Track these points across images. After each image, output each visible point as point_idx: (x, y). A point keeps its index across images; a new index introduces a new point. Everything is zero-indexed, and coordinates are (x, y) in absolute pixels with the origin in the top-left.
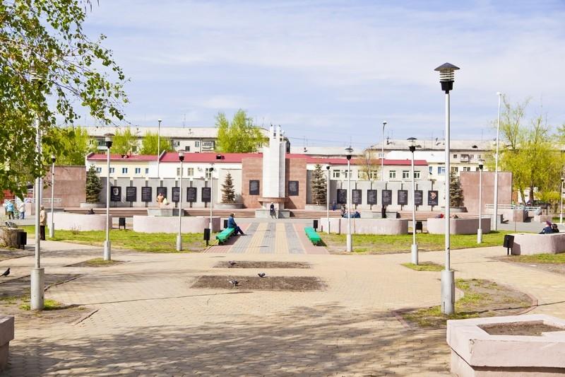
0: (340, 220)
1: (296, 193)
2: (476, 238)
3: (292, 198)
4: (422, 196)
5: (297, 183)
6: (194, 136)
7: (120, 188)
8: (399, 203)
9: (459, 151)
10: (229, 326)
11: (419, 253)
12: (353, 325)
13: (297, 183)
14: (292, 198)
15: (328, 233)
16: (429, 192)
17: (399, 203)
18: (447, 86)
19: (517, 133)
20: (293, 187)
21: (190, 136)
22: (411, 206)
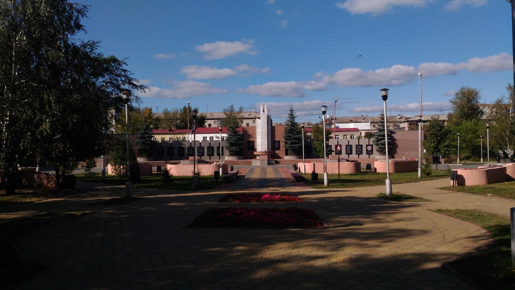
0: (314, 164)
1: (279, 149)
2: (418, 173)
3: (277, 152)
4: (362, 148)
5: (279, 142)
6: (214, 117)
7: (341, 146)
8: (346, 154)
9: (376, 122)
10: (313, 243)
11: (392, 185)
12: (311, 263)
13: (279, 142)
14: (277, 152)
15: (304, 172)
16: (367, 146)
17: (346, 154)
18: (385, 98)
19: (452, 118)
20: (276, 144)
21: (211, 118)
22: (364, 155)
